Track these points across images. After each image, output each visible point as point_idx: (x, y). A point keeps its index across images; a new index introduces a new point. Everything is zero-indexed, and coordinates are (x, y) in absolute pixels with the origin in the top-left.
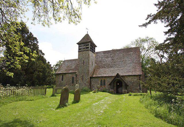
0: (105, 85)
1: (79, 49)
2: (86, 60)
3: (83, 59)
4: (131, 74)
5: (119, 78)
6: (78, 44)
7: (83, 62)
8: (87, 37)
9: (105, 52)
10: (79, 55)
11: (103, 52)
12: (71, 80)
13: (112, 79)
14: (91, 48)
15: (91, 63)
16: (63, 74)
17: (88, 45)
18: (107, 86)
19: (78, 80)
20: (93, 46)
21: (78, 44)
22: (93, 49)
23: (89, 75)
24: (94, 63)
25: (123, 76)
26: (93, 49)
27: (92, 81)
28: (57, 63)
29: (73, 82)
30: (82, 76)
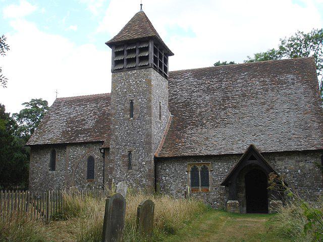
0: (206, 183)
1: (116, 63)
2: (139, 101)
3: (129, 96)
4: (294, 147)
5: (254, 161)
6: (110, 44)
7: (128, 106)
8: (141, 20)
9: (199, 73)
10: (114, 83)
11: (193, 71)
12: (84, 167)
13: (233, 165)
14: (155, 60)
15: (155, 111)
16: (54, 148)
17: (147, 49)
18: (215, 188)
19: (112, 169)
20: (163, 52)
21: (110, 44)
22: (161, 64)
23: (150, 150)
24: (165, 108)
25: (265, 154)
26: (161, 64)
27: (162, 172)
28: (24, 107)
29: (91, 175)
30: (127, 153)
